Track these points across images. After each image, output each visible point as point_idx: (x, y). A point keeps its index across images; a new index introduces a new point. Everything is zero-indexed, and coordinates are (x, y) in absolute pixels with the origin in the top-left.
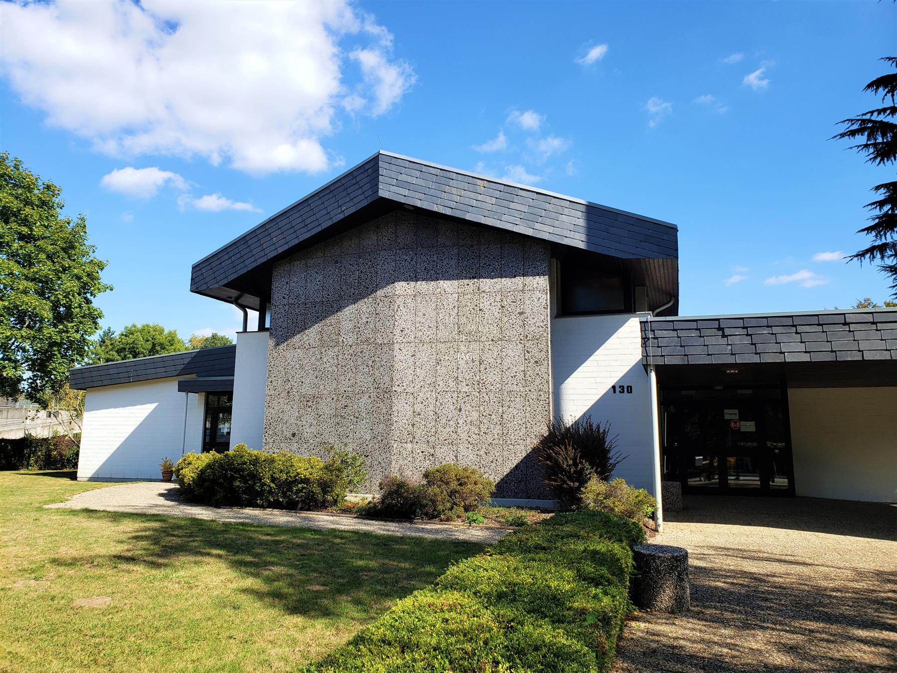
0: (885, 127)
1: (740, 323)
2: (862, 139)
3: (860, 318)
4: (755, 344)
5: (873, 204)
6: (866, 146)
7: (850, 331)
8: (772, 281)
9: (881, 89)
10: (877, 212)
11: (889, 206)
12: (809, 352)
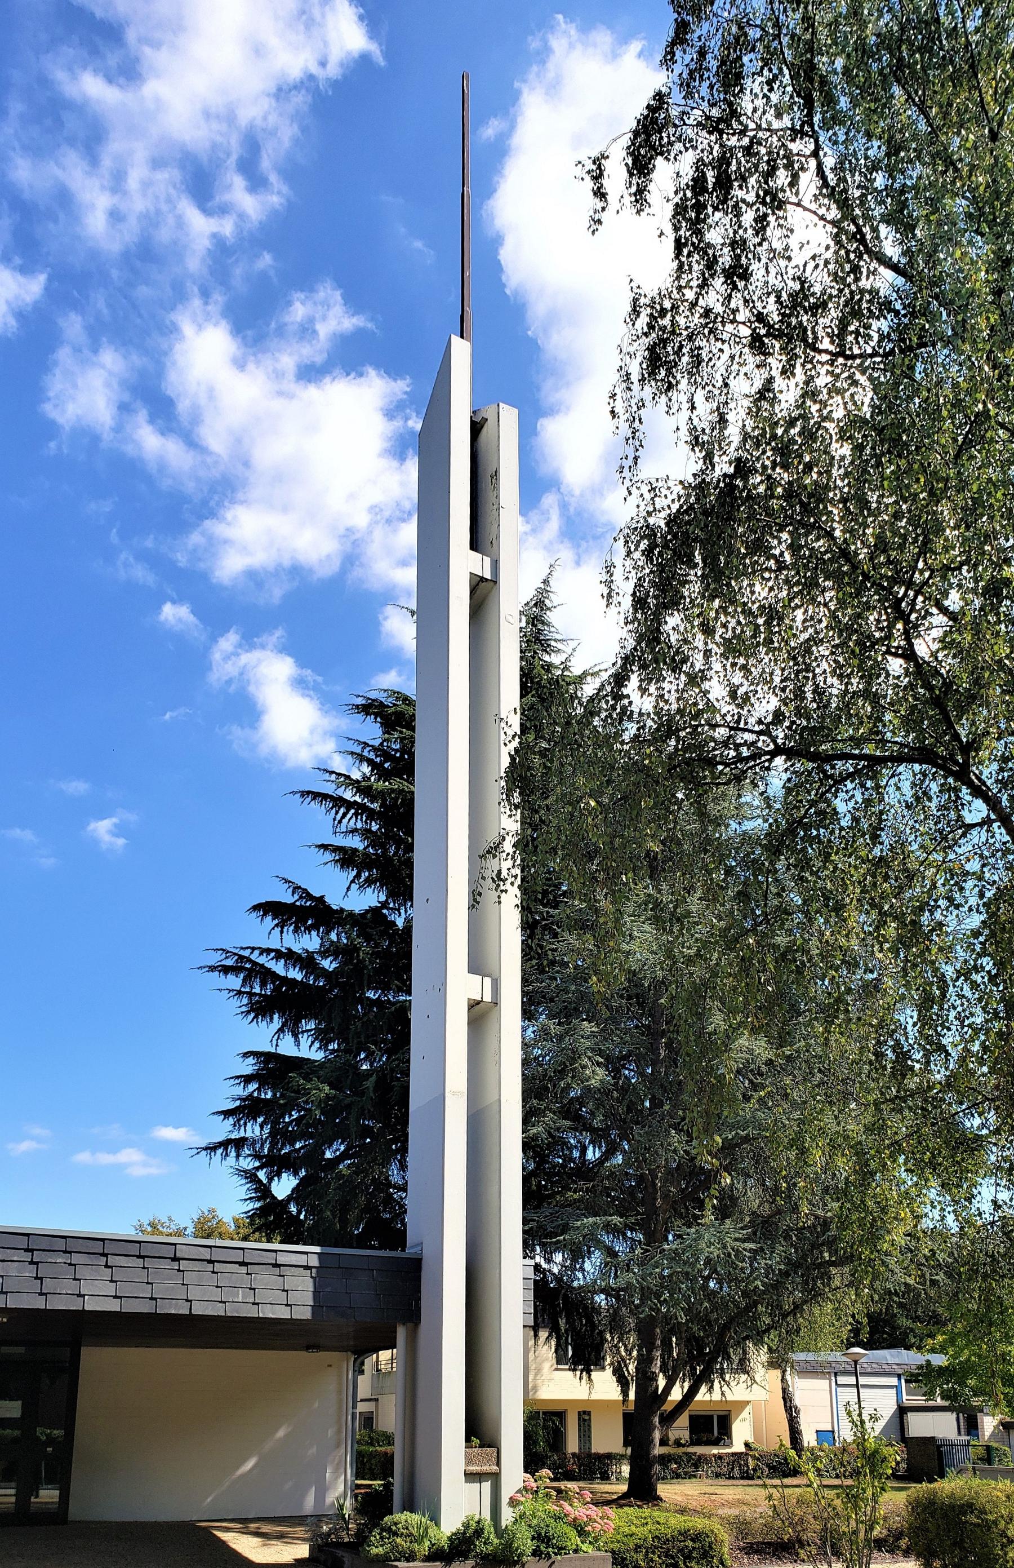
0: (266, 975)
1: (23, 1242)
2: (235, 982)
3: (195, 1253)
4: (41, 1279)
5: (237, 1077)
6: (239, 993)
7: (179, 1270)
8: (84, 1157)
9: (269, 918)
10: (240, 1091)
11: (256, 1086)
12: (120, 1297)
